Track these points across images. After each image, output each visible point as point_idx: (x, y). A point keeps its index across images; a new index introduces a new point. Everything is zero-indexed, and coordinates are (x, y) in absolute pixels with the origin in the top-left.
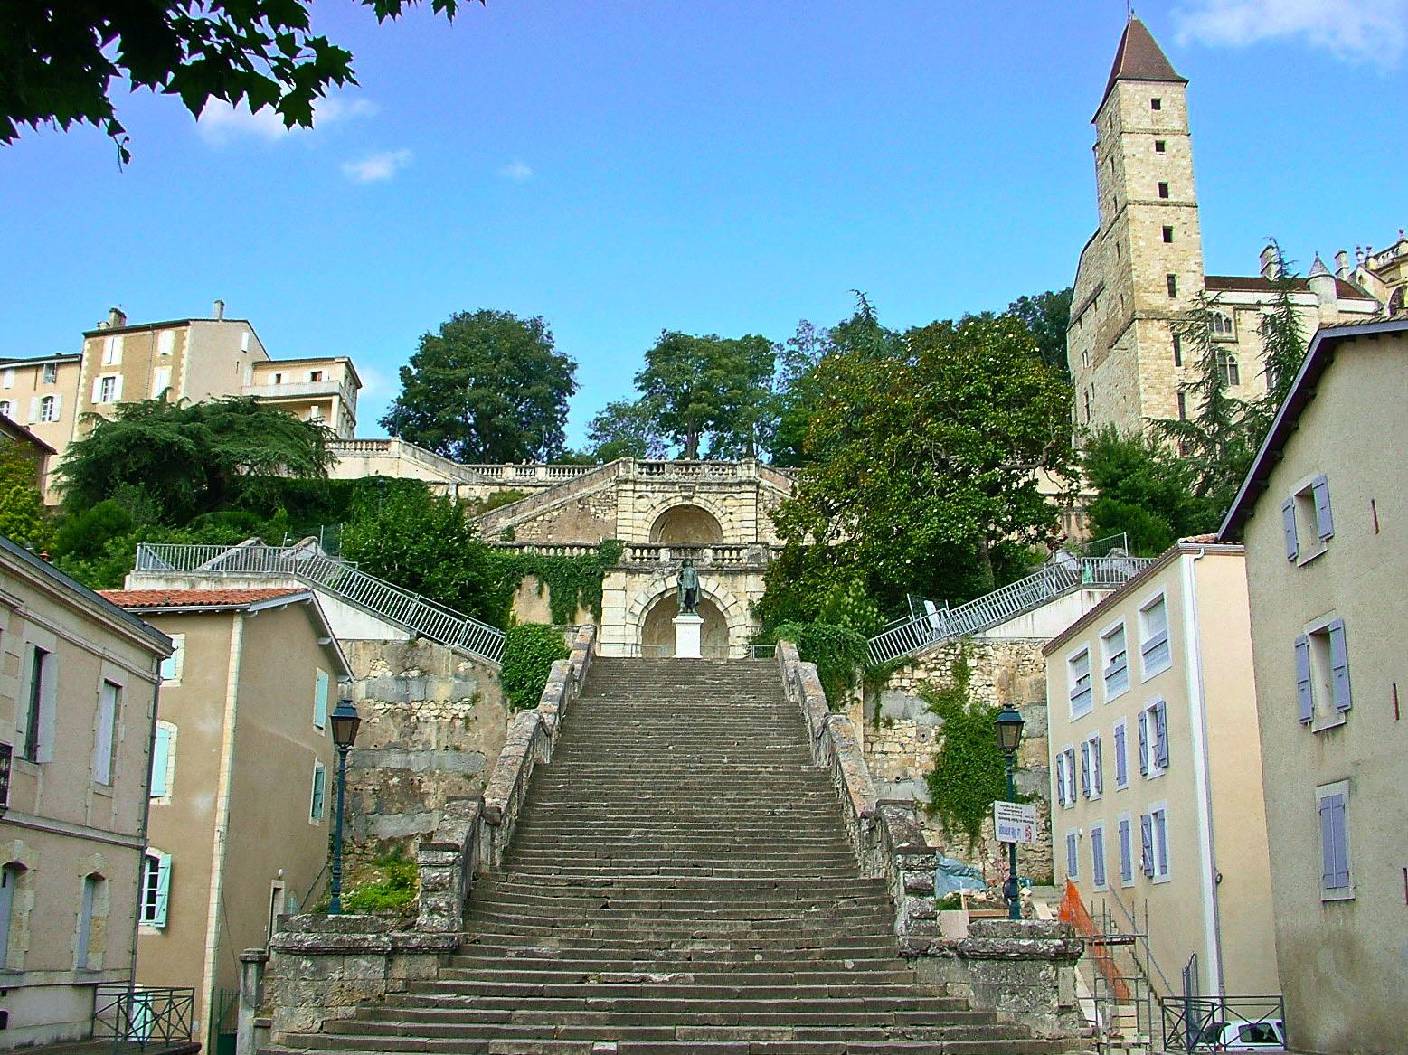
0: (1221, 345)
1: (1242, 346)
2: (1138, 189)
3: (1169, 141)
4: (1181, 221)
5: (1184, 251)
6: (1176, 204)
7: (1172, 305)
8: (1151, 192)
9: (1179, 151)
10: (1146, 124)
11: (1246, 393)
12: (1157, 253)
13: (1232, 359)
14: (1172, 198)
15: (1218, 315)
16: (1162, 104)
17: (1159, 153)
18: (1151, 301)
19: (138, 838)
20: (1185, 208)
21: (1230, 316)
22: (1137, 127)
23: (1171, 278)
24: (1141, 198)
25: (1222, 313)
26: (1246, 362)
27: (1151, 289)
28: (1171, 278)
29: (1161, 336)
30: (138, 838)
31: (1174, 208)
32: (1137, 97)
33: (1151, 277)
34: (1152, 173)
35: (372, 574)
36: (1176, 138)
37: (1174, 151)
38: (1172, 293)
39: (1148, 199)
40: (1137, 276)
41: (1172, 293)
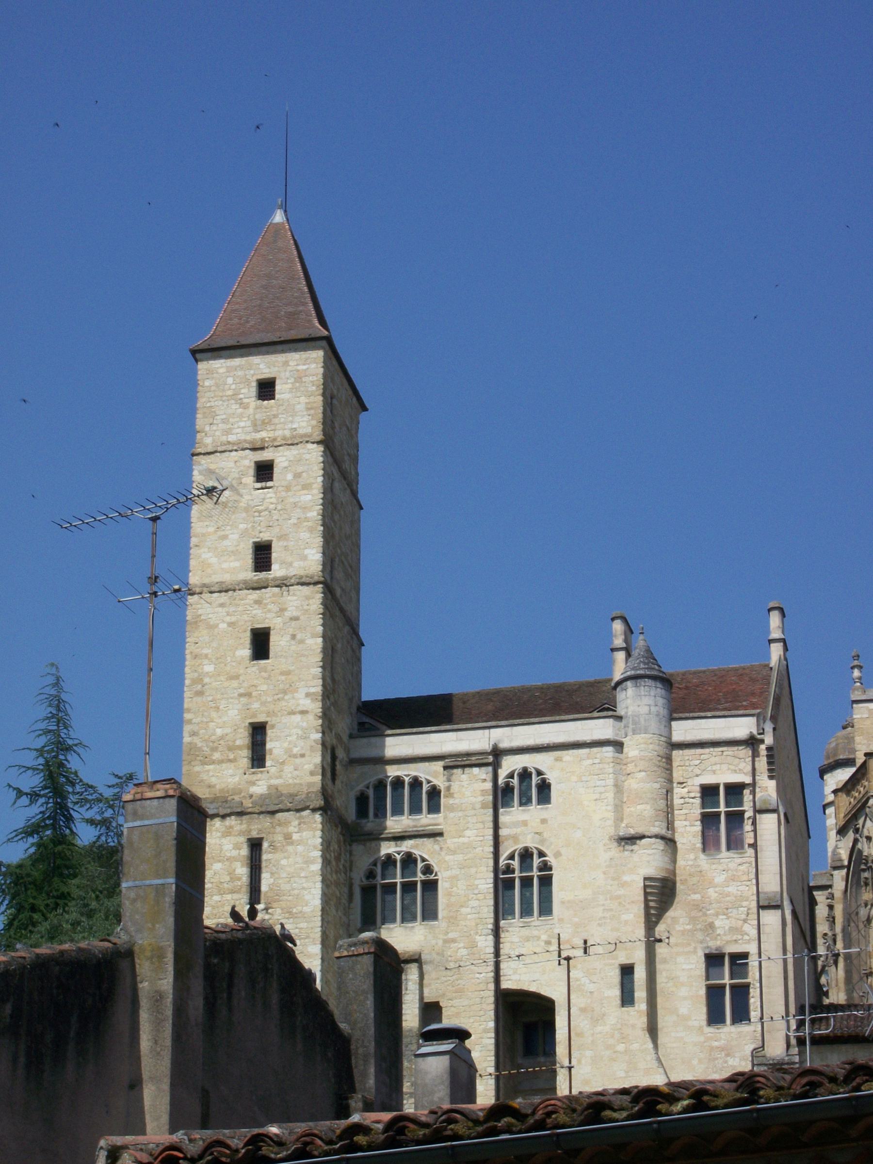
0: (407, 846)
1: (449, 841)
2: (214, 560)
3: (281, 459)
4: (288, 614)
5: (237, 677)
6: (283, 584)
7: (253, 783)
8: (237, 564)
9: (297, 476)
10: (242, 432)
11: (451, 935)
12: (235, 684)
13: (428, 870)
14: (277, 570)
15: (416, 783)
16: (278, 387)
17: (259, 485)
18: (214, 780)
19: (755, 755)
20: (300, 587)
21: (440, 782)
22: (224, 438)
23: (258, 731)
24: (216, 578)
25: (423, 777)
26: (455, 872)
27: (217, 756)
28: (258, 731)
29: (226, 847)
30: (755, 755)
31: (277, 590)
32: (230, 380)
33: (219, 732)
34: (242, 526)
35: (746, 708)
36: (294, 451)
37: (290, 477)
38: (258, 758)
39: (227, 578)
40: (194, 734)
41: (258, 758)
